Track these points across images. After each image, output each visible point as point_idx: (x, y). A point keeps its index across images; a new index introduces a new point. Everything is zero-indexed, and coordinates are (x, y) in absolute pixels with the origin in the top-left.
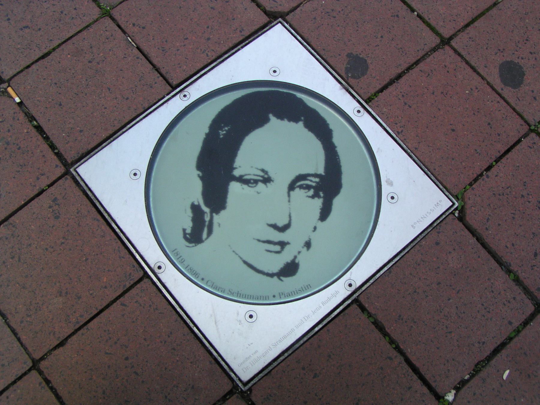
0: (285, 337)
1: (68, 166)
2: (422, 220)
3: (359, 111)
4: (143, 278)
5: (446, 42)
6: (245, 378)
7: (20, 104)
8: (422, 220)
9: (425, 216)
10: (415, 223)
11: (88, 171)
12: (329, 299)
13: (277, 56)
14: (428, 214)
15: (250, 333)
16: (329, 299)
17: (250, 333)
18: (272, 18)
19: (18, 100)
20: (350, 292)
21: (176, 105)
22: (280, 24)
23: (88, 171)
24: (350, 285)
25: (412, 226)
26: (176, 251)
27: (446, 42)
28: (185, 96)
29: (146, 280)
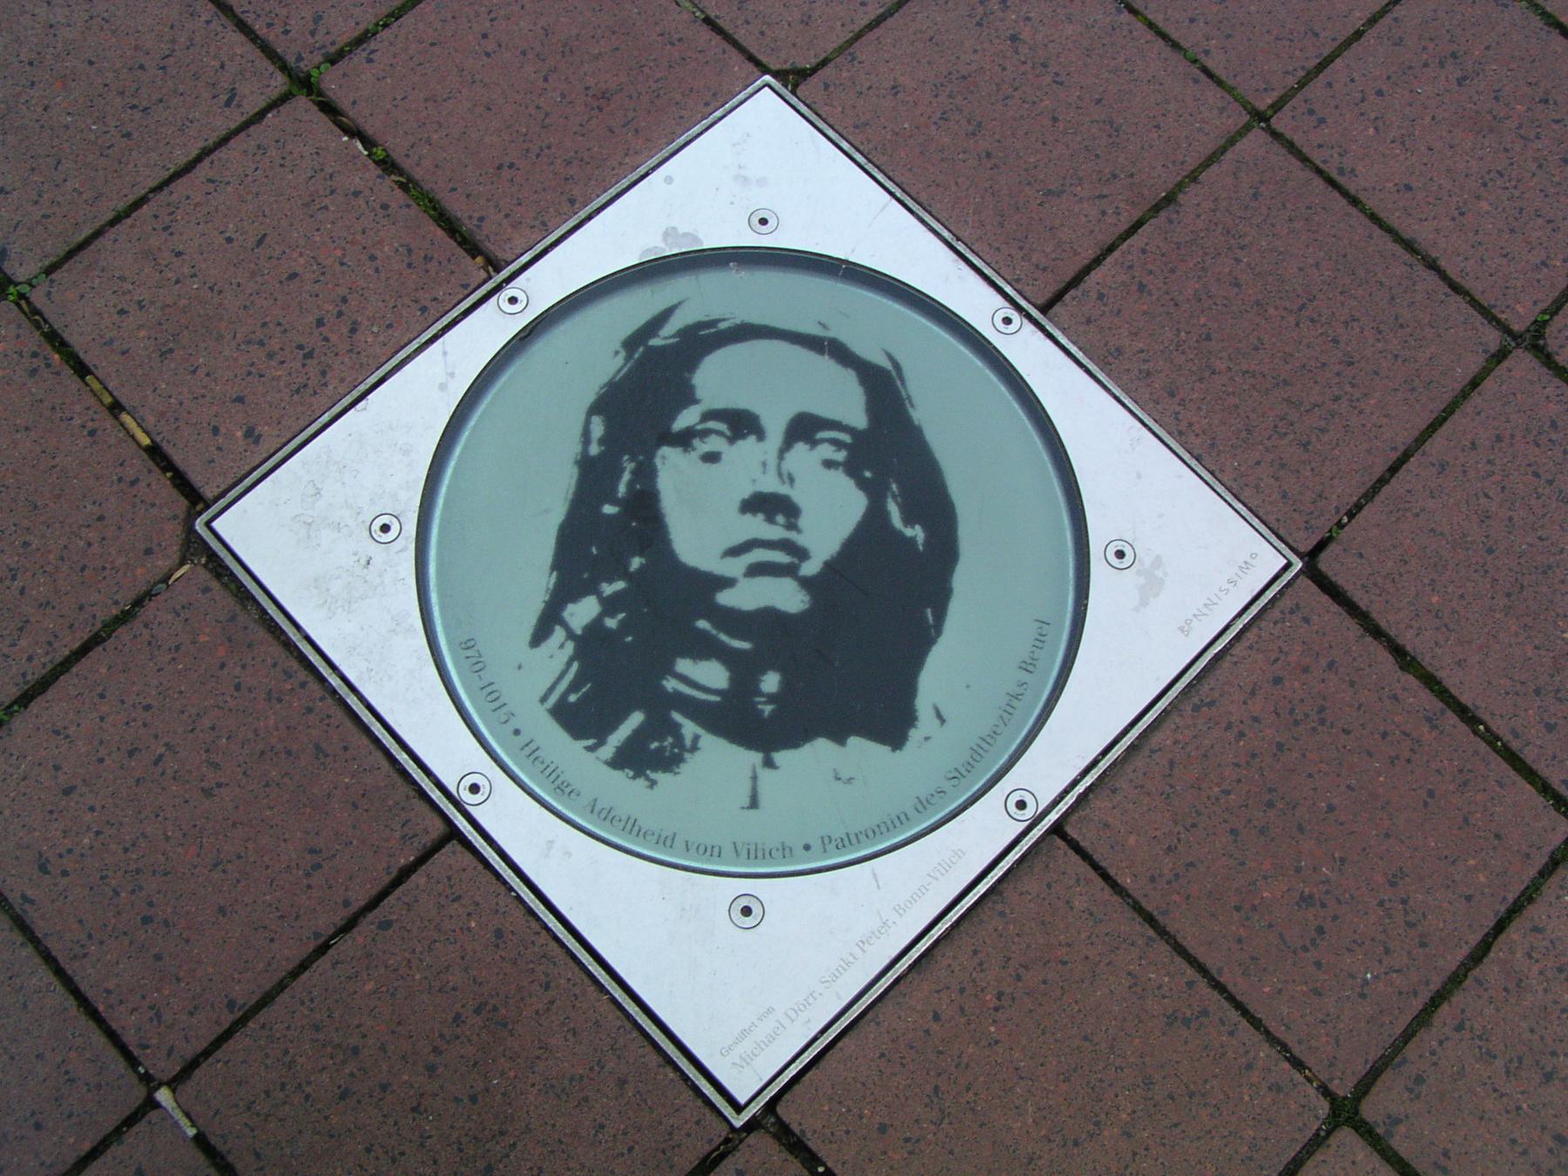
2: (1205, 611)
8: (1205, 611)
10: (1188, 622)
11: (254, 529)
15: (746, 941)
17: (746, 941)
23: (254, 529)
25: (1182, 629)
27: (1534, 340)
28: (513, 300)
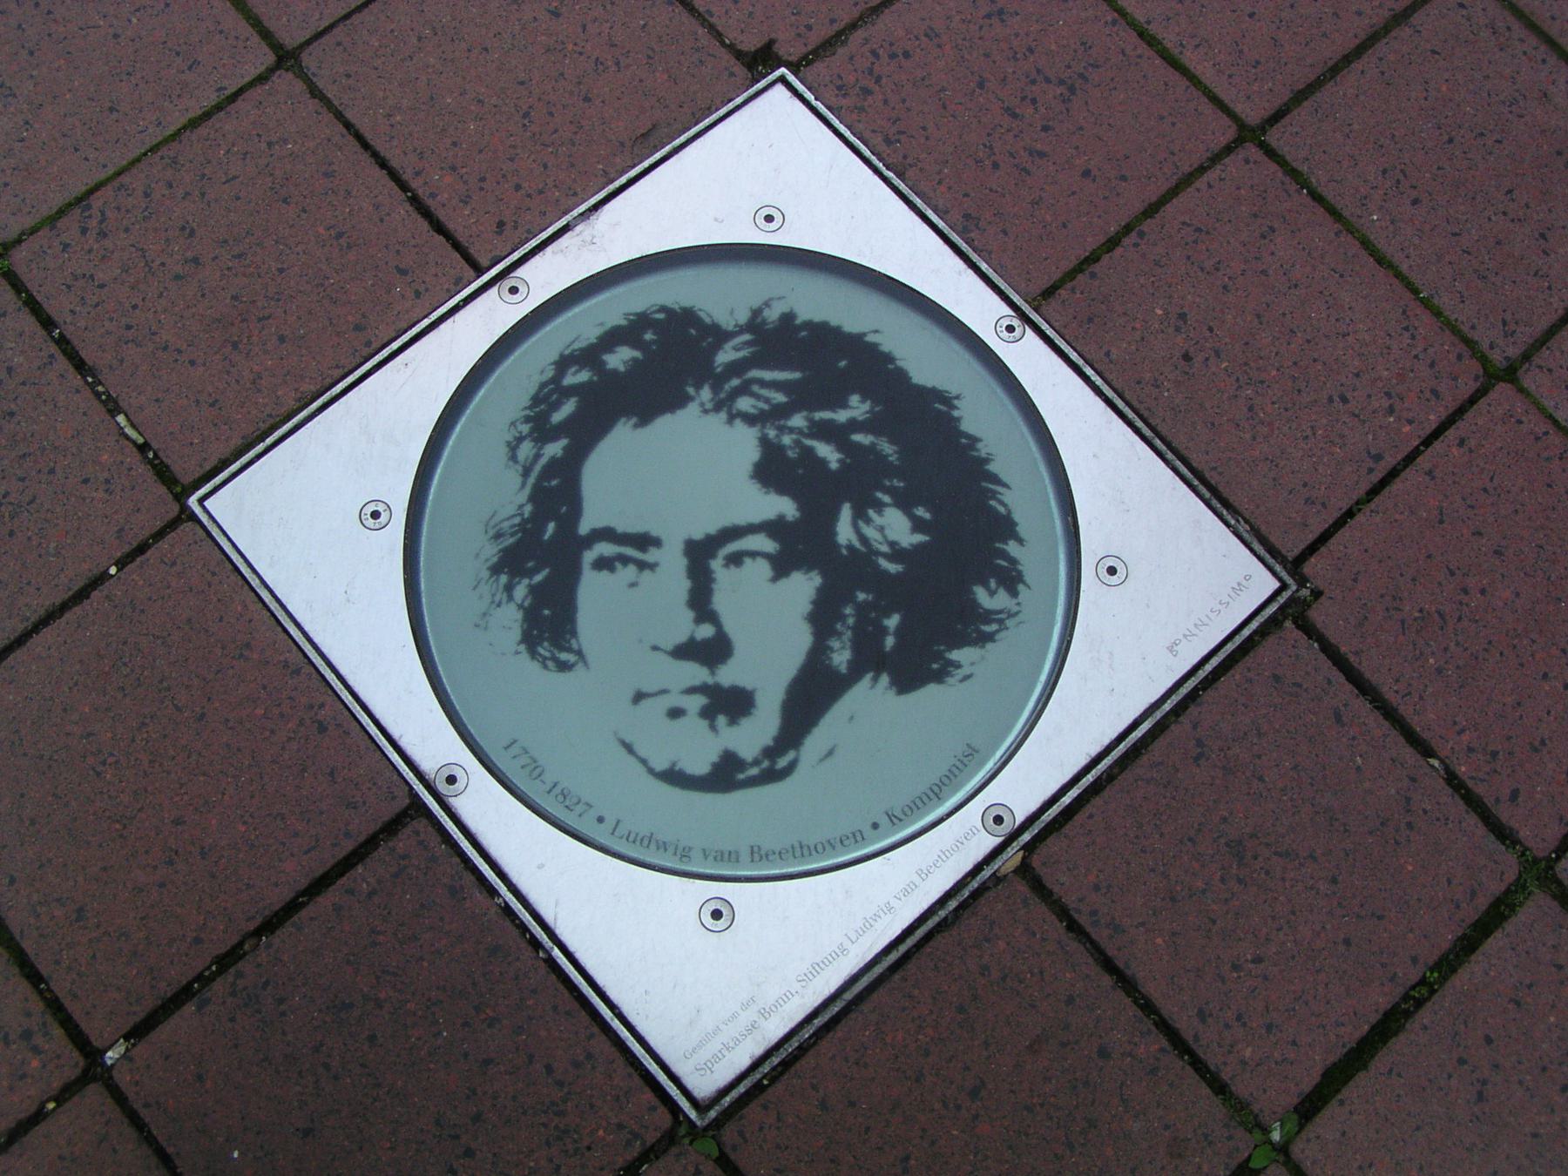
0: (835, 956)
1: (179, 482)
3: (1010, 329)
4: (410, 816)
5: (1248, 135)
6: (704, 1084)
7: (113, 407)
8: (1195, 631)
9: (1206, 620)
12: (924, 874)
13: (773, 177)
14: (1212, 616)
15: (708, 963)
16: (944, 855)
17: (708, 963)
18: (758, 63)
19: (121, 419)
20: (999, 840)
21: (490, 316)
22: (780, 88)
24: (998, 820)
25: (1170, 649)
26: (557, 790)
28: (514, 290)
29: (188, 526)
